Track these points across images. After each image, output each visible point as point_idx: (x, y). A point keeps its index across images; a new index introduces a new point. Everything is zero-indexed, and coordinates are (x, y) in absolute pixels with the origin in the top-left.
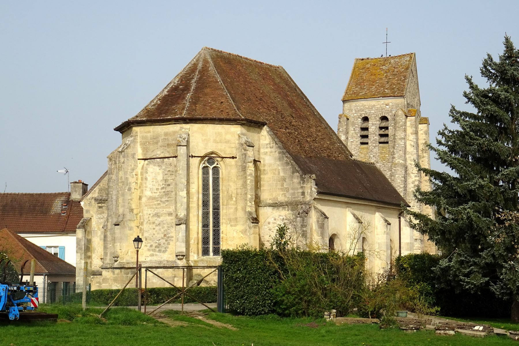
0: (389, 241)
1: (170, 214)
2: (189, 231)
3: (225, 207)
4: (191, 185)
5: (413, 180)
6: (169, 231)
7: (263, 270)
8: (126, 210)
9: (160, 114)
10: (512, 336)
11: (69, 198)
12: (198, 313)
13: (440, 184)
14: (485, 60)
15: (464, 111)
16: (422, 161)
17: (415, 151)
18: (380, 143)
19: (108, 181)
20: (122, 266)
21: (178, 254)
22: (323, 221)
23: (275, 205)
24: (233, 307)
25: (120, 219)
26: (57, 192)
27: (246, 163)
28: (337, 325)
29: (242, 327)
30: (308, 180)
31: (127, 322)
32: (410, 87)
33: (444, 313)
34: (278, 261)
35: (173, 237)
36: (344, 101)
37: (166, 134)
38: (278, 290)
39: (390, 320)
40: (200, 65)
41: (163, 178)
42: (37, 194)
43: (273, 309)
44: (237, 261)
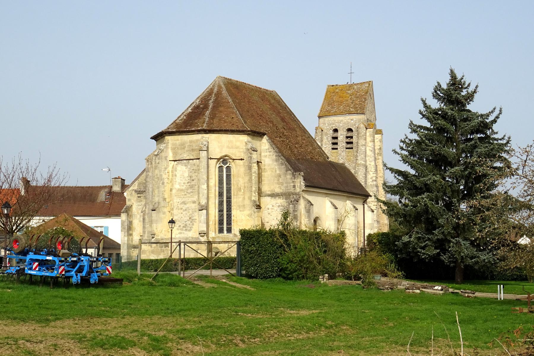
0: (357, 222)
1: (194, 202)
2: (208, 215)
3: (235, 197)
4: (210, 180)
5: (372, 176)
6: (193, 215)
7: (271, 245)
8: (160, 199)
9: (186, 126)
10: (463, 294)
11: (111, 190)
12: (221, 277)
13: (402, 179)
14: (436, 86)
15: (420, 125)
16: (378, 162)
17: (373, 154)
18: (347, 148)
19: (146, 177)
20: (158, 241)
21: (200, 233)
22: (310, 207)
23: (273, 195)
24: (249, 272)
25: (156, 206)
26: (102, 185)
27: (251, 164)
28: (329, 285)
29: (258, 288)
30: (298, 176)
31: (173, 284)
32: (369, 107)
33: (408, 277)
34: (283, 238)
35: (196, 219)
36: (320, 117)
37: (191, 142)
38: (284, 259)
39: (370, 282)
40: (216, 90)
41: (189, 174)
42: (86, 187)
43: (280, 274)
44: (252, 238)
